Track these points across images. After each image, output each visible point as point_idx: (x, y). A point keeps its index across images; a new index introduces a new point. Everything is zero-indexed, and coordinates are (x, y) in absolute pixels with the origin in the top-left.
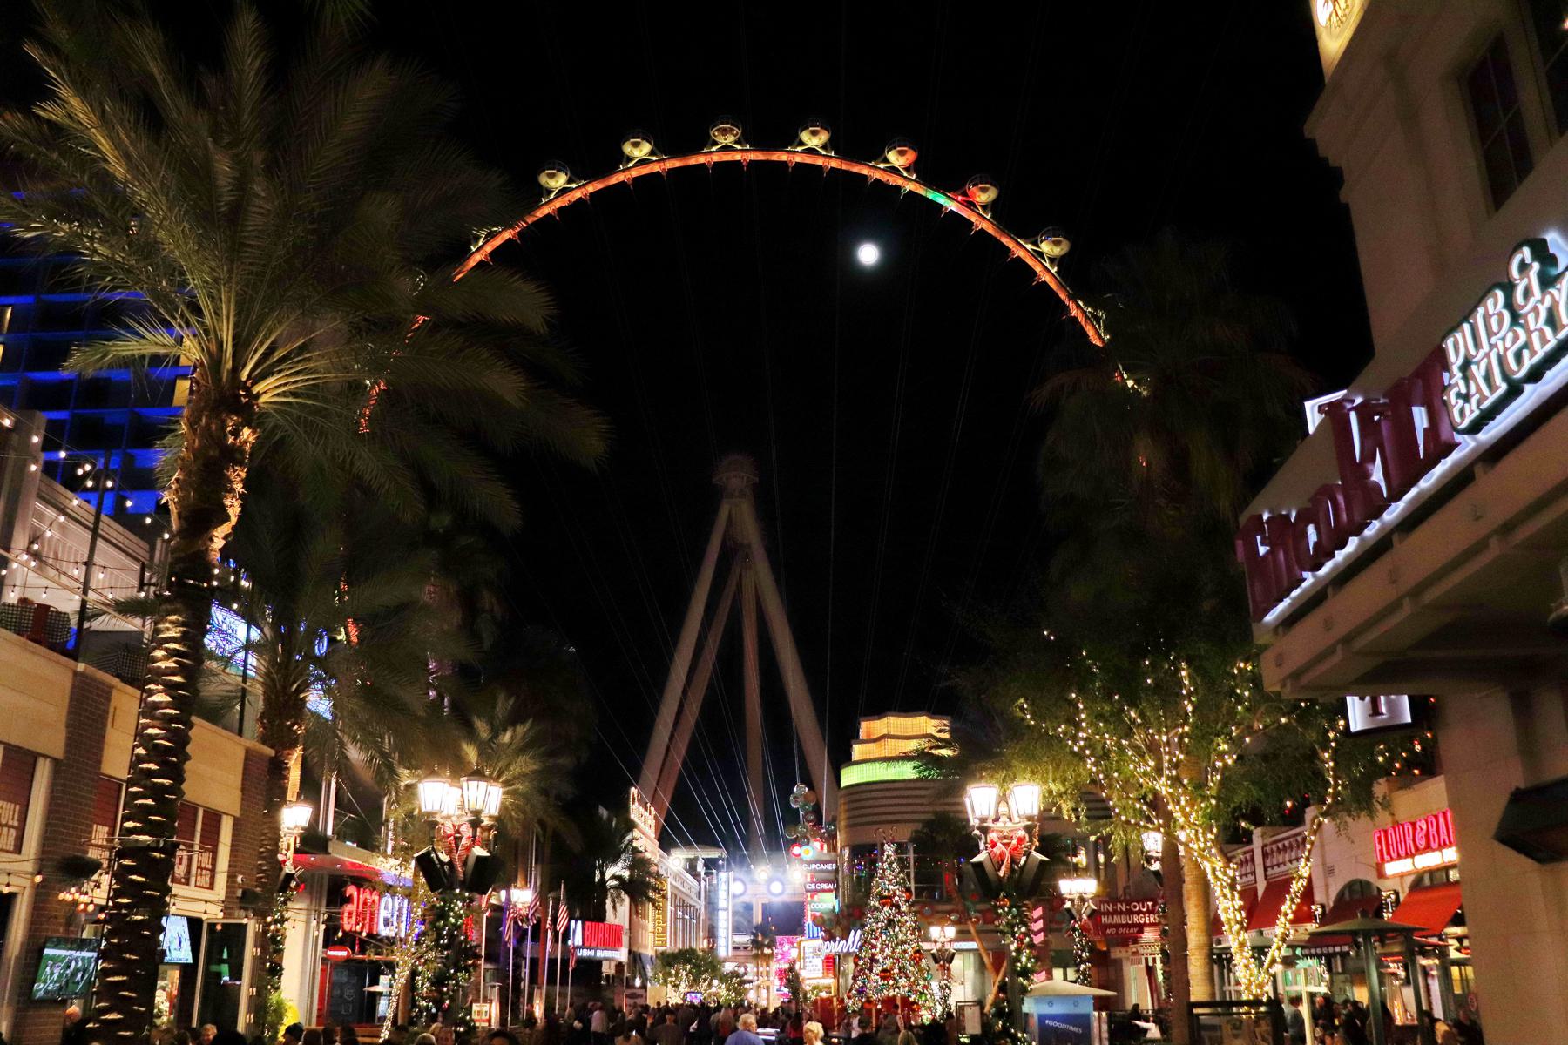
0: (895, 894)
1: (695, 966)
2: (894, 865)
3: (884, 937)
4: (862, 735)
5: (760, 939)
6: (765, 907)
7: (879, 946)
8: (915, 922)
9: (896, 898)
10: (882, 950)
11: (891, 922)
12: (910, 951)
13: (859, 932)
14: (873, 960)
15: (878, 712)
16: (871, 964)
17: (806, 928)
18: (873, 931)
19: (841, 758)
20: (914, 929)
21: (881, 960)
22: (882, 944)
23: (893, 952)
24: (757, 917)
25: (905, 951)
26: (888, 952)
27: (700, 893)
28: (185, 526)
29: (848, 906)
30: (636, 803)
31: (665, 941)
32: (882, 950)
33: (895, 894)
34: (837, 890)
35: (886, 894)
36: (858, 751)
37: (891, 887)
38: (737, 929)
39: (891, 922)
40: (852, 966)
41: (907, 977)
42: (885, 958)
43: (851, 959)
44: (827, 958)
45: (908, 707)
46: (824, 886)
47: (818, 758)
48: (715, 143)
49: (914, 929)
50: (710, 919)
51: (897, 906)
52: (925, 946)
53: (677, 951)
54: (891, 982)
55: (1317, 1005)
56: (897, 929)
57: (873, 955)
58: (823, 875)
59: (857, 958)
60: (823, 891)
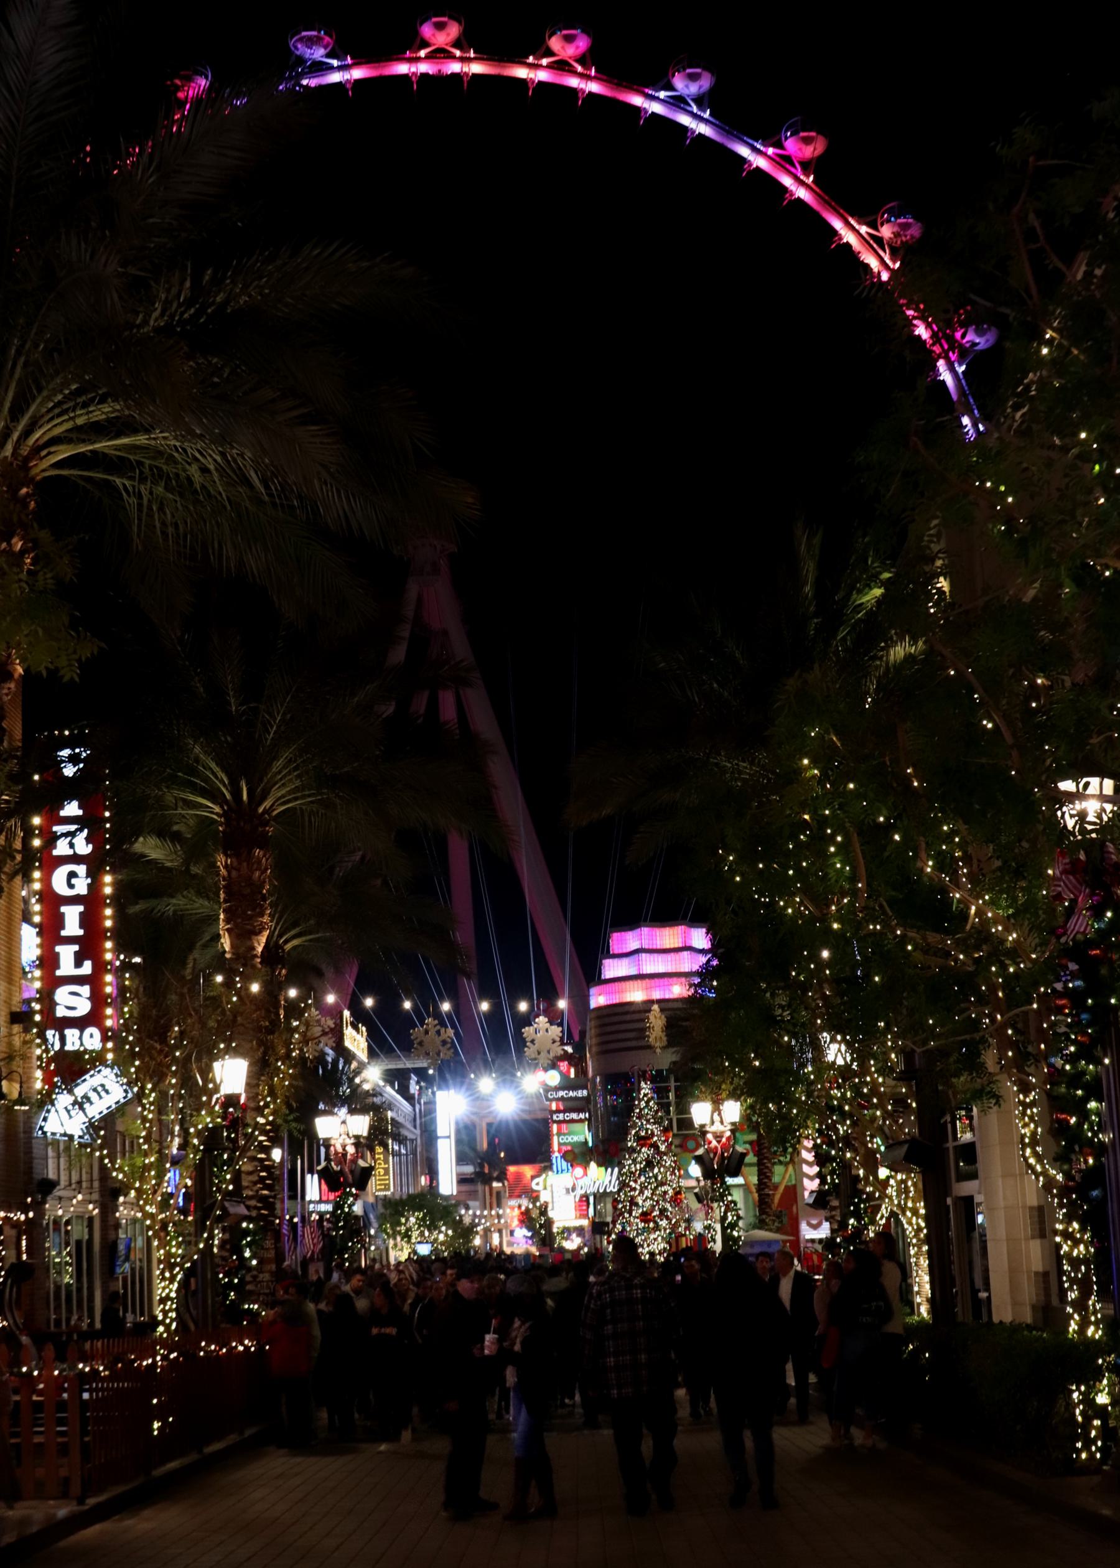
0: (653, 1134)
1: (430, 1213)
2: (651, 1103)
3: (643, 1179)
4: (615, 948)
5: (486, 1171)
6: (489, 1125)
7: (638, 1187)
8: (675, 1162)
9: (655, 1139)
10: (642, 1192)
11: (650, 1164)
12: (671, 1192)
13: (616, 1170)
14: (633, 1202)
15: (631, 923)
16: (631, 1206)
17: (554, 1161)
18: (631, 1173)
19: (592, 976)
20: (674, 1169)
21: (640, 1203)
22: (640, 1185)
23: (652, 1194)
24: (482, 1145)
25: (665, 1193)
26: (647, 1193)
27: (415, 1120)
28: (568, 1256)
29: (603, 1142)
30: (349, 1027)
31: (389, 1185)
32: (642, 1192)
33: (653, 1134)
34: (589, 1120)
35: (643, 1134)
36: (612, 969)
37: (648, 1126)
38: (461, 1159)
39: (650, 1164)
40: (609, 1207)
41: (667, 1218)
42: (644, 1201)
43: (609, 1201)
44: (582, 1196)
45: (665, 917)
46: (574, 1116)
47: (565, 971)
48: (425, 44)
49: (674, 1169)
50: (427, 1151)
51: (655, 1146)
52: (684, 1183)
53: (405, 1197)
54: (651, 1225)
55: (916, 314)
56: (656, 1170)
57: (633, 1198)
58: (570, 1104)
59: (616, 1202)
60: (572, 1121)
